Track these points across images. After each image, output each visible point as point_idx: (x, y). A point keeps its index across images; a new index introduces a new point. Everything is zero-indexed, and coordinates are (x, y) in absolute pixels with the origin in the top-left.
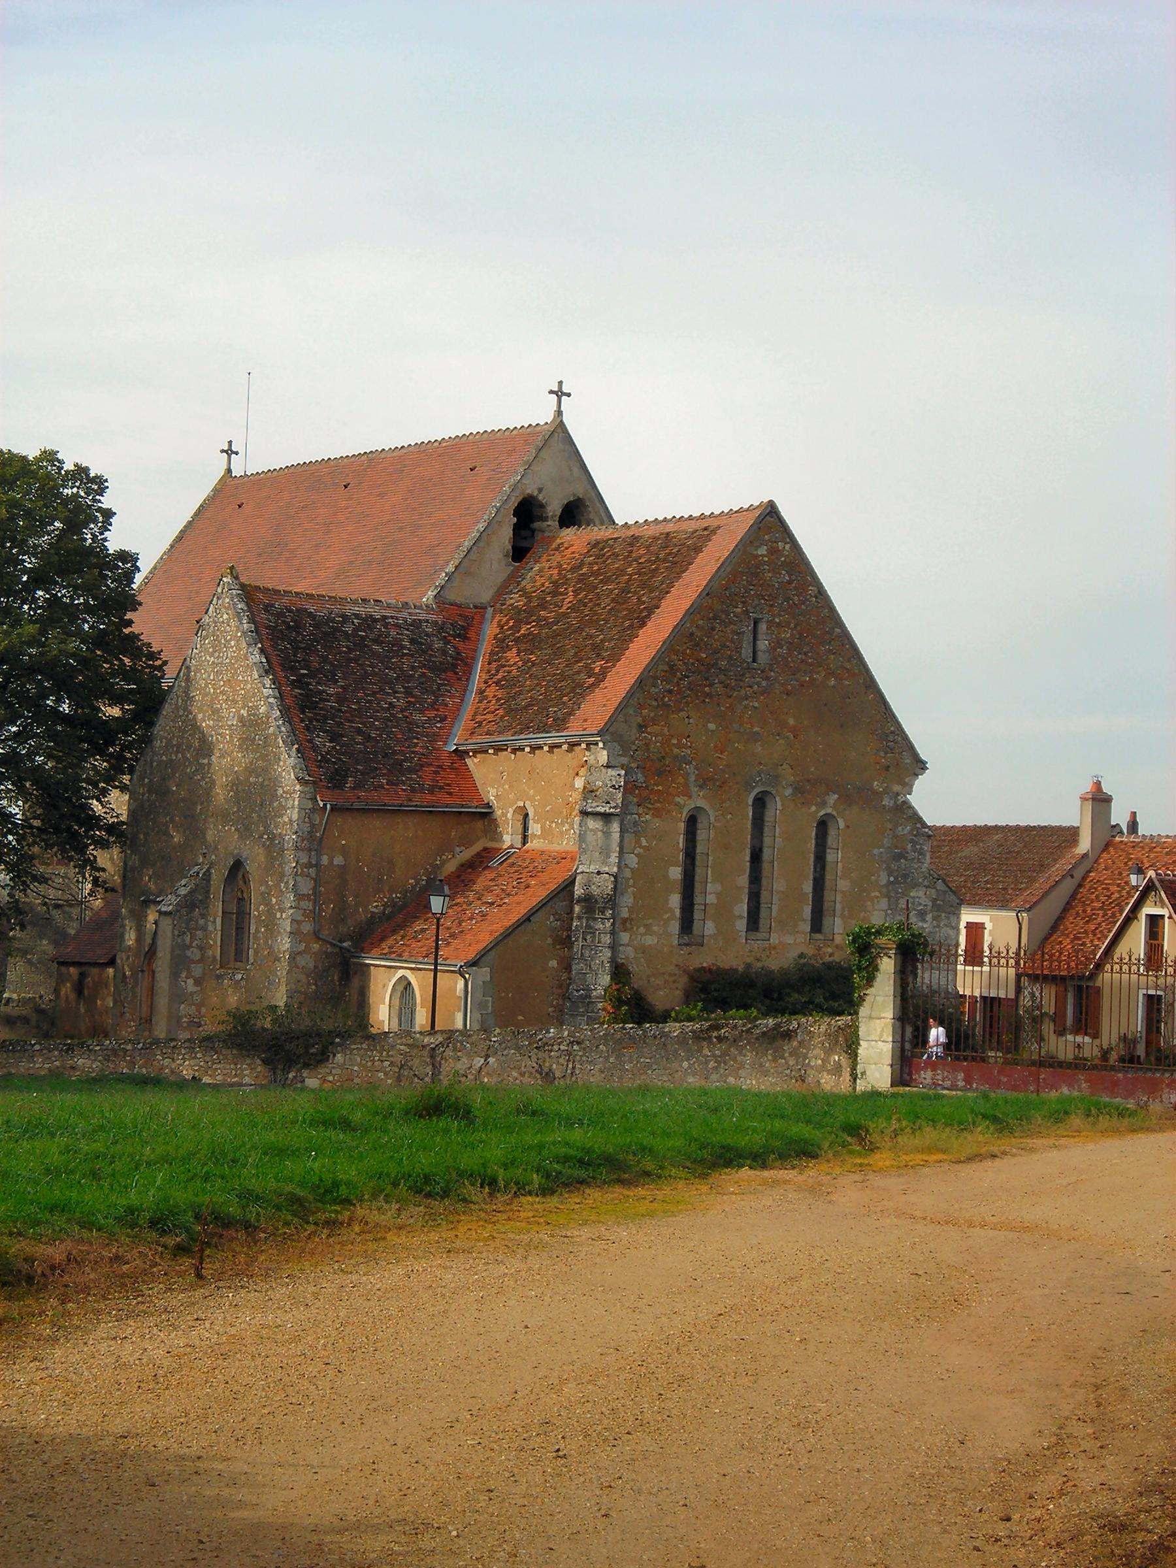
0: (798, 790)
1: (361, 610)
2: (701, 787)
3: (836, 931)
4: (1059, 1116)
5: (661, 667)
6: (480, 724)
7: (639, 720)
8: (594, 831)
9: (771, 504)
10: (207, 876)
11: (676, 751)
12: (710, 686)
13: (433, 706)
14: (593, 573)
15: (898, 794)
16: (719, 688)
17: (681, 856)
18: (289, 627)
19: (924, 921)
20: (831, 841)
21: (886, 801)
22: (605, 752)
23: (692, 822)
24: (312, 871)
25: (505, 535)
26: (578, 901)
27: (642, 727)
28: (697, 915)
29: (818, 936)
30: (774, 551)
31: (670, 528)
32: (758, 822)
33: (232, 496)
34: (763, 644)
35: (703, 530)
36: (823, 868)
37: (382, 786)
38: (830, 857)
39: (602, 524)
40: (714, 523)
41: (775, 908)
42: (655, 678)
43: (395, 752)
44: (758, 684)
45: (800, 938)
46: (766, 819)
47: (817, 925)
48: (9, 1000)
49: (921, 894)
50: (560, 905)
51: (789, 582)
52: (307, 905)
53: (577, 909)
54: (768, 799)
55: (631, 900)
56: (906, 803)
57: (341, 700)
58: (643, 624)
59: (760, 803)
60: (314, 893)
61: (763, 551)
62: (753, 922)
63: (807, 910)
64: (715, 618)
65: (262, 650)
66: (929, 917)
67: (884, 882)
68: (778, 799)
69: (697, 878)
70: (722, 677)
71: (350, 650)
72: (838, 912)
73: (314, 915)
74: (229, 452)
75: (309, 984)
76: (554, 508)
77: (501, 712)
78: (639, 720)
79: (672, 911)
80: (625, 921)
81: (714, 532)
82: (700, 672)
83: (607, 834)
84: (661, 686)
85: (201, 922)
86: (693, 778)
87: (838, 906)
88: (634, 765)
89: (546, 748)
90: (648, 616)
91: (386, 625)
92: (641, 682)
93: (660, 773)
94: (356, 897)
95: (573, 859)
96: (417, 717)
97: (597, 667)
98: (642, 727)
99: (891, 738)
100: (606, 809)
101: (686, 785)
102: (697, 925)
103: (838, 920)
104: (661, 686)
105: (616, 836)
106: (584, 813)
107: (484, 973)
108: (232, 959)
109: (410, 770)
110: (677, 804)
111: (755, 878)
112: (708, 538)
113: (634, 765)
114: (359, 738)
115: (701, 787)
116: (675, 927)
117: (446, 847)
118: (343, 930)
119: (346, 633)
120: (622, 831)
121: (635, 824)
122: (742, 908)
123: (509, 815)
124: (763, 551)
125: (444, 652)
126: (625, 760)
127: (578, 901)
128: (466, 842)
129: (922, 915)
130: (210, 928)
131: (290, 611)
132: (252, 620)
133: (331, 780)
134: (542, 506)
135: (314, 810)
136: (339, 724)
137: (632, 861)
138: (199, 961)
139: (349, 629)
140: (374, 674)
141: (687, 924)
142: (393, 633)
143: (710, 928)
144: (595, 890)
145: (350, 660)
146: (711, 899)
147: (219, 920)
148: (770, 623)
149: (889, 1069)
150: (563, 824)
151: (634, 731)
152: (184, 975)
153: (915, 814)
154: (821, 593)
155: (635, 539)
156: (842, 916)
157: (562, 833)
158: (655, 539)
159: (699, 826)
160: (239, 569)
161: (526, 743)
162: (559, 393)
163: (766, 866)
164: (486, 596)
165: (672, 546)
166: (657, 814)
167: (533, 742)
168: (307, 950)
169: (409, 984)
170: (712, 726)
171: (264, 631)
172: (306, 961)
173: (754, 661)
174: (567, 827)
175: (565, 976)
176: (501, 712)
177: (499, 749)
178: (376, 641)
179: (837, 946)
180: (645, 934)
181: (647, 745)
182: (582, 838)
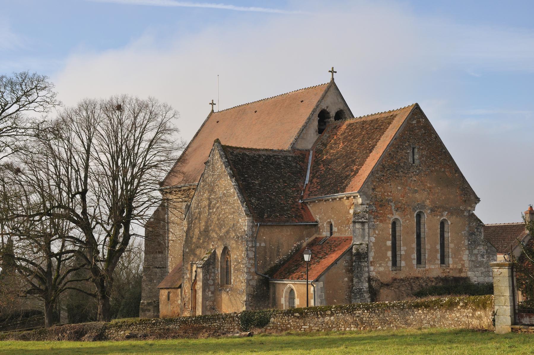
0: (432, 210)
2: (397, 211)
3: (450, 263)
4: (274, 293)
5: (379, 167)
6: (311, 192)
7: (373, 186)
8: (359, 229)
9: (417, 105)
11: (387, 198)
12: (398, 173)
13: (293, 187)
14: (349, 135)
15: (470, 211)
16: (401, 173)
17: (391, 237)
18: (240, 160)
19: (483, 258)
20: (446, 229)
21: (466, 214)
22: (361, 199)
23: (394, 224)
24: (254, 249)
26: (354, 255)
27: (373, 189)
28: (398, 259)
29: (443, 265)
30: (418, 122)
31: (378, 116)
32: (419, 223)
33: (213, 119)
34: (417, 157)
35: (390, 117)
36: (444, 239)
37: (277, 216)
38: (446, 235)
41: (427, 255)
42: (378, 171)
44: (416, 172)
45: (437, 266)
46: (421, 222)
47: (443, 261)
48: (143, 303)
49: (481, 248)
50: (347, 257)
51: (425, 133)
52: (252, 262)
53: (354, 258)
54: (422, 215)
55: (373, 254)
56: (473, 214)
57: (260, 185)
58: (371, 152)
59: (419, 216)
60: (255, 257)
61: (414, 122)
62: (419, 261)
63: (439, 256)
64: (398, 148)
65: (231, 169)
66: (485, 257)
67: (467, 244)
68: (425, 214)
69: (397, 245)
70: (402, 170)
72: (450, 256)
73: (255, 265)
74: (213, 104)
75: (254, 291)
76: (333, 114)
77: (319, 187)
78: (373, 186)
79: (388, 258)
80: (371, 262)
81: (395, 116)
82: (394, 168)
83: (364, 230)
85: (213, 270)
86: (393, 207)
87: (450, 254)
88: (372, 203)
89: (338, 199)
90: (373, 149)
91: (275, 158)
92: (372, 173)
93: (381, 206)
94: (270, 258)
95: (351, 240)
96: (288, 190)
97: (355, 168)
98: (373, 189)
99: (466, 190)
101: (391, 210)
102: (398, 262)
103: (450, 259)
105: (367, 230)
107: (321, 284)
108: (225, 283)
109: (287, 210)
110: (388, 218)
111: (419, 244)
112: (393, 119)
113: (372, 203)
114: (268, 199)
115: (397, 211)
116: (390, 264)
117: (301, 238)
118: (266, 270)
119: (261, 162)
120: (369, 228)
121: (373, 225)
122: (415, 256)
123: (325, 225)
124: (414, 122)
125: (296, 167)
126: (368, 202)
127: (354, 255)
128: (309, 236)
129: (482, 256)
130: (216, 272)
131: (240, 154)
132: (226, 158)
135: (253, 226)
136: (260, 194)
137: (373, 239)
138: (213, 285)
139: (261, 160)
140: (271, 176)
141: (394, 263)
143: (403, 263)
146: (403, 253)
147: (219, 269)
148: (419, 149)
149: (510, 318)
150: (346, 227)
151: (371, 191)
152: (207, 290)
153: (477, 218)
154: (437, 137)
155: (364, 122)
156: (452, 257)
157: (345, 230)
158: (372, 121)
159: (397, 225)
160: (221, 140)
161: (330, 197)
162: (333, 72)
163: (422, 240)
164: (310, 147)
165: (376, 125)
166: (381, 221)
167: (333, 197)
168: (253, 279)
169: (292, 289)
170: (399, 188)
171: (231, 162)
172: (253, 283)
173: (413, 163)
174: (347, 228)
175: (350, 284)
176: (319, 187)
177: (319, 201)
178: (272, 164)
179: (451, 269)
180: (379, 267)
181: (376, 196)
182: (354, 231)
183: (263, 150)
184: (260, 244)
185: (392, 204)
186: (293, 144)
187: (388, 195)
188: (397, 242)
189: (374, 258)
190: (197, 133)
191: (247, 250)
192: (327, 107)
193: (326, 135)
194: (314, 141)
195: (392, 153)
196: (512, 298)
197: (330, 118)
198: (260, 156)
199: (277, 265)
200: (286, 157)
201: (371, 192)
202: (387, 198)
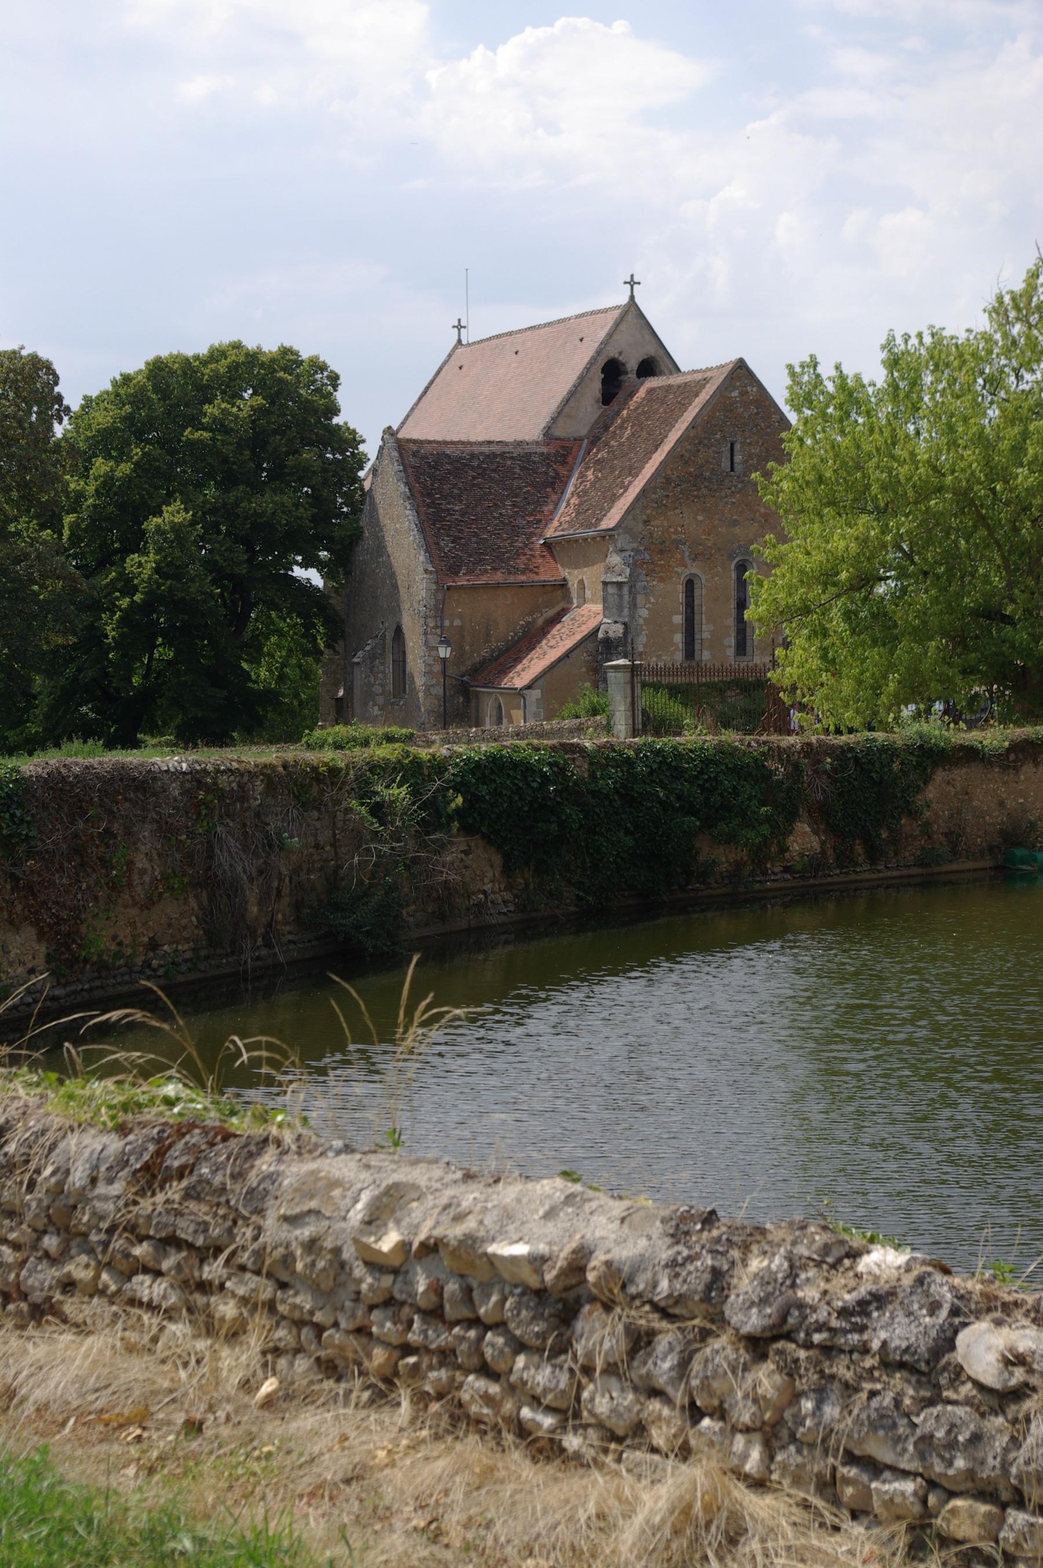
1: (485, 449)
4: (477, 710)
10: (384, 636)
12: (698, 490)
16: (705, 491)
18: (430, 466)
23: (690, 585)
24: (438, 631)
25: (596, 386)
28: (697, 647)
34: (738, 458)
39: (671, 373)
40: (709, 374)
42: (656, 488)
43: (499, 547)
51: (757, 414)
57: (464, 513)
61: (735, 394)
71: (474, 478)
78: (645, 517)
79: (676, 644)
83: (621, 596)
84: (660, 492)
86: (687, 554)
98: (646, 522)
100: (620, 579)
102: (697, 653)
104: (660, 492)
105: (626, 598)
106: (605, 584)
115: (694, 560)
118: (463, 669)
121: (645, 588)
124: (735, 394)
126: (635, 545)
133: (449, 569)
134: (623, 364)
135: (437, 590)
139: (475, 463)
140: (490, 493)
142: (509, 463)
144: (611, 634)
145: (474, 485)
146: (706, 635)
148: (743, 443)
162: (632, 283)
166: (662, 580)
170: (700, 518)
171: (410, 470)
181: (651, 534)
183: (481, 444)
184: (452, 622)
185: (685, 548)
186: (547, 432)
187: (676, 532)
188: (696, 617)
189: (645, 646)
190: (427, 389)
191: (425, 633)
192: (620, 353)
193: (615, 405)
194: (593, 420)
195: (687, 455)
196: (629, 714)
197: (626, 373)
198: (473, 456)
199: (484, 659)
200: (527, 457)
201: (640, 527)
202: (674, 537)
